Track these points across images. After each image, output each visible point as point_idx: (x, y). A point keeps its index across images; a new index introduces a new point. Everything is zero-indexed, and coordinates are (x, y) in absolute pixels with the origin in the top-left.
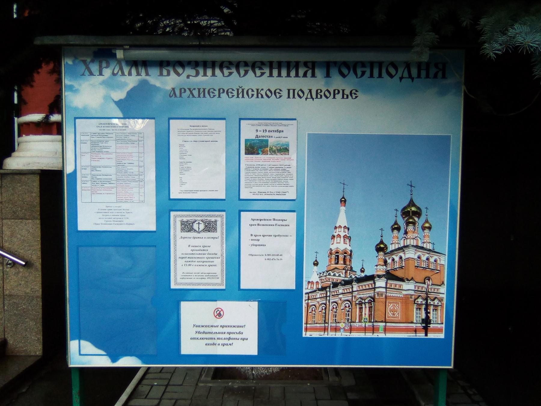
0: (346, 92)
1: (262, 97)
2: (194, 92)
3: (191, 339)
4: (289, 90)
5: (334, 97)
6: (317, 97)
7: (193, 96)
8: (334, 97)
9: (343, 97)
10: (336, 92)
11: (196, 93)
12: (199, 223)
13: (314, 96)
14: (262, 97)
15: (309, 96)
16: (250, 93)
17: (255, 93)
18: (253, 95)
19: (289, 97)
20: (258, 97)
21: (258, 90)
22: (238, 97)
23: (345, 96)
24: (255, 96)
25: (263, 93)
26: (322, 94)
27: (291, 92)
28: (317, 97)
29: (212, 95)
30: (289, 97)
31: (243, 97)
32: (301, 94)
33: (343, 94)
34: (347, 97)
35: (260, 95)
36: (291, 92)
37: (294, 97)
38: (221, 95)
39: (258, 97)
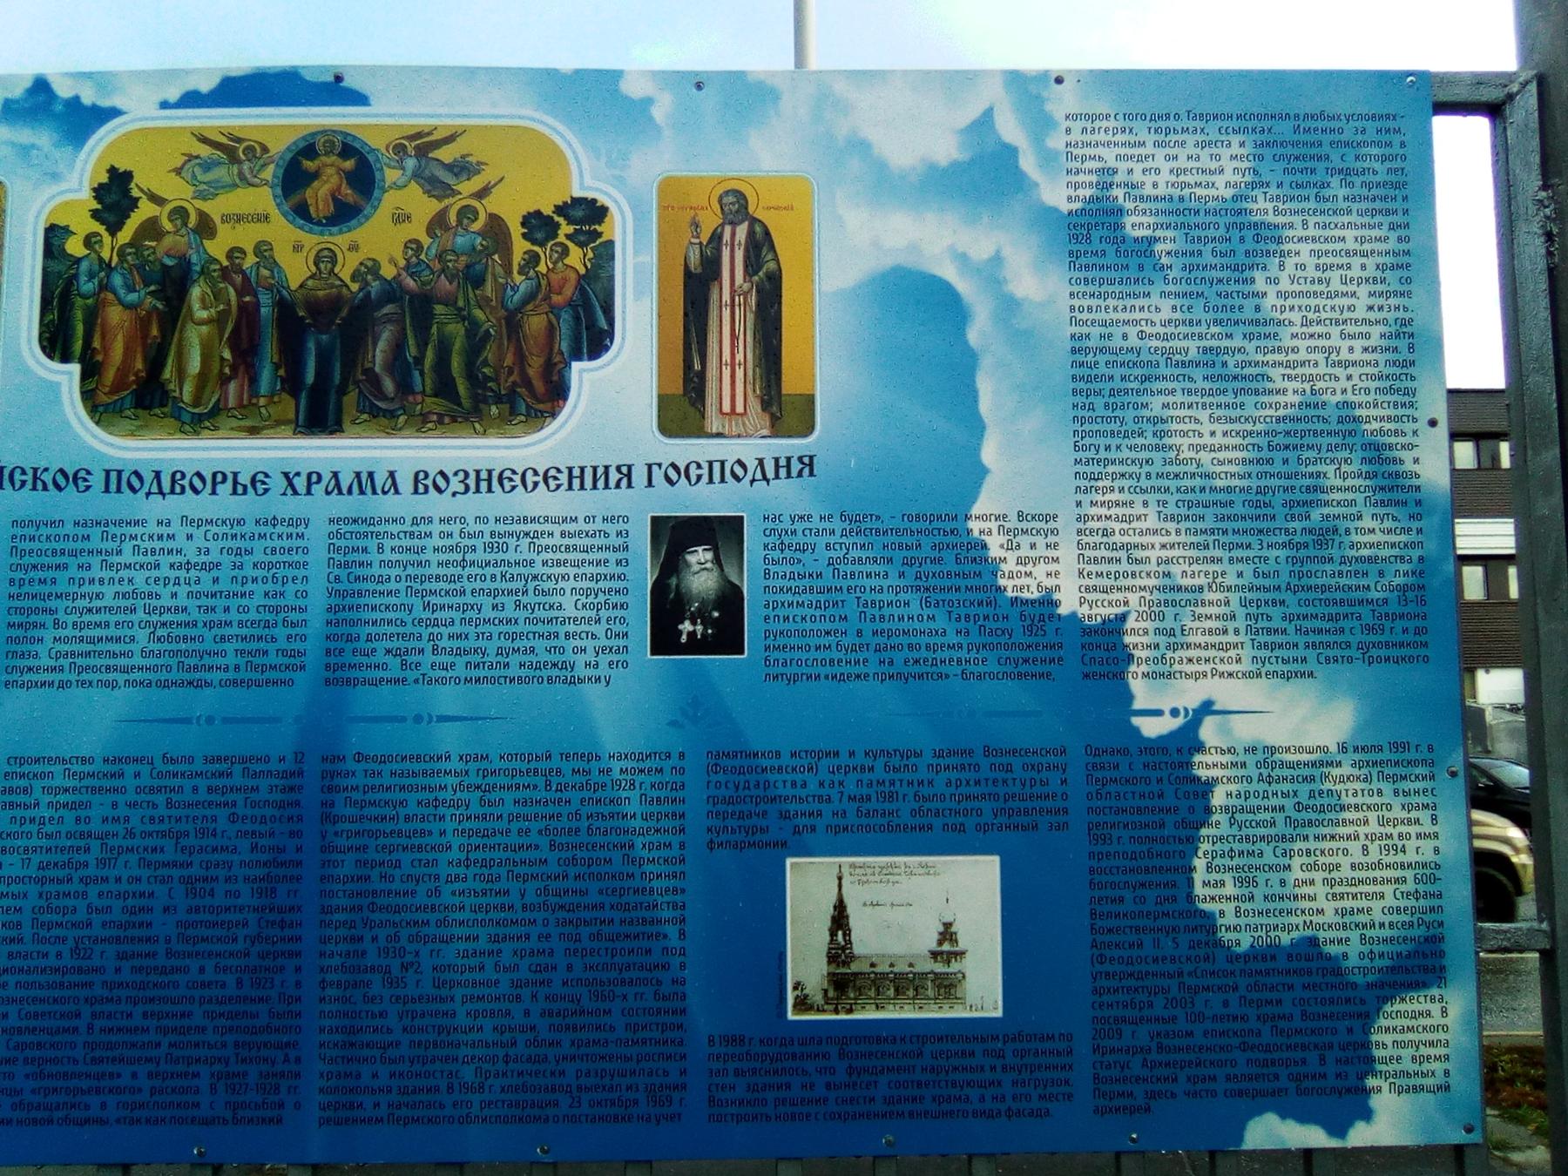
0: (241, 479)
1: (45, 488)
2: (296, 481)
3: (790, 208)
4: (108, 472)
5: (214, 492)
6: (172, 492)
7: (295, 492)
8: (214, 492)
9: (235, 492)
10: (219, 478)
11: (300, 483)
12: (1493, 883)
13: (166, 488)
14: (45, 488)
15: (155, 489)
16: (18, 476)
17: (29, 478)
18: (23, 483)
19: (107, 490)
20: (34, 488)
21: (35, 470)
22: (570, 488)
23: (240, 489)
24: (29, 485)
25: (47, 477)
26: (429, 482)
27: (113, 475)
28: (172, 492)
29: (507, 485)
30: (107, 490)
31: (490, 490)
32: (136, 483)
33: (235, 482)
34: (245, 492)
35: (40, 485)
36: (113, 475)
37: (119, 490)
38: (220, 488)
39: (34, 488)
